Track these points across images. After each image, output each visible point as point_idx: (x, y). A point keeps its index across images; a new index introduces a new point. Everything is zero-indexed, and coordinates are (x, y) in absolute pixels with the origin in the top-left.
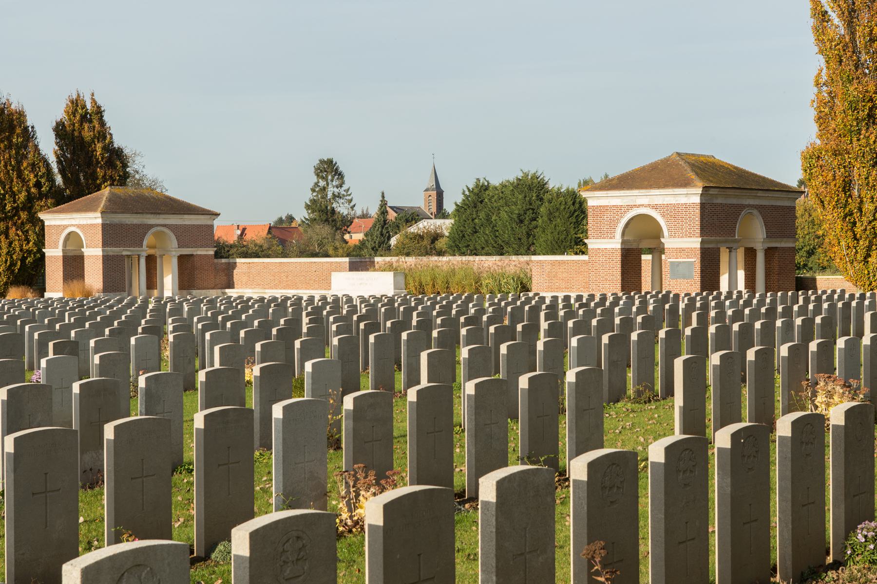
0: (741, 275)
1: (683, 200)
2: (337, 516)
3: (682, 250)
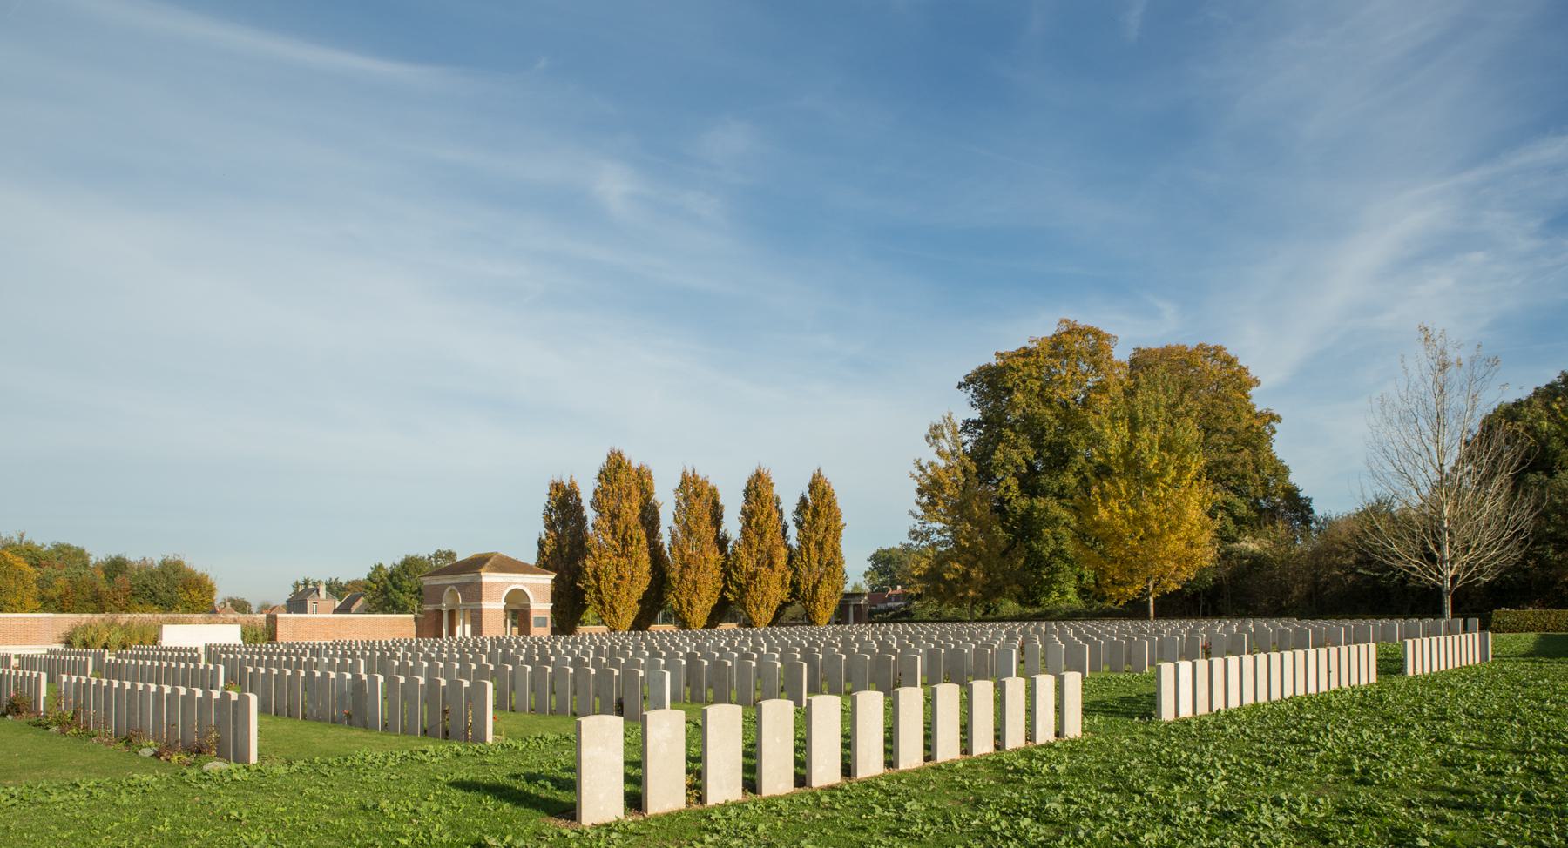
0: (468, 627)
1: (541, 582)
2: (1290, 592)
3: (540, 610)
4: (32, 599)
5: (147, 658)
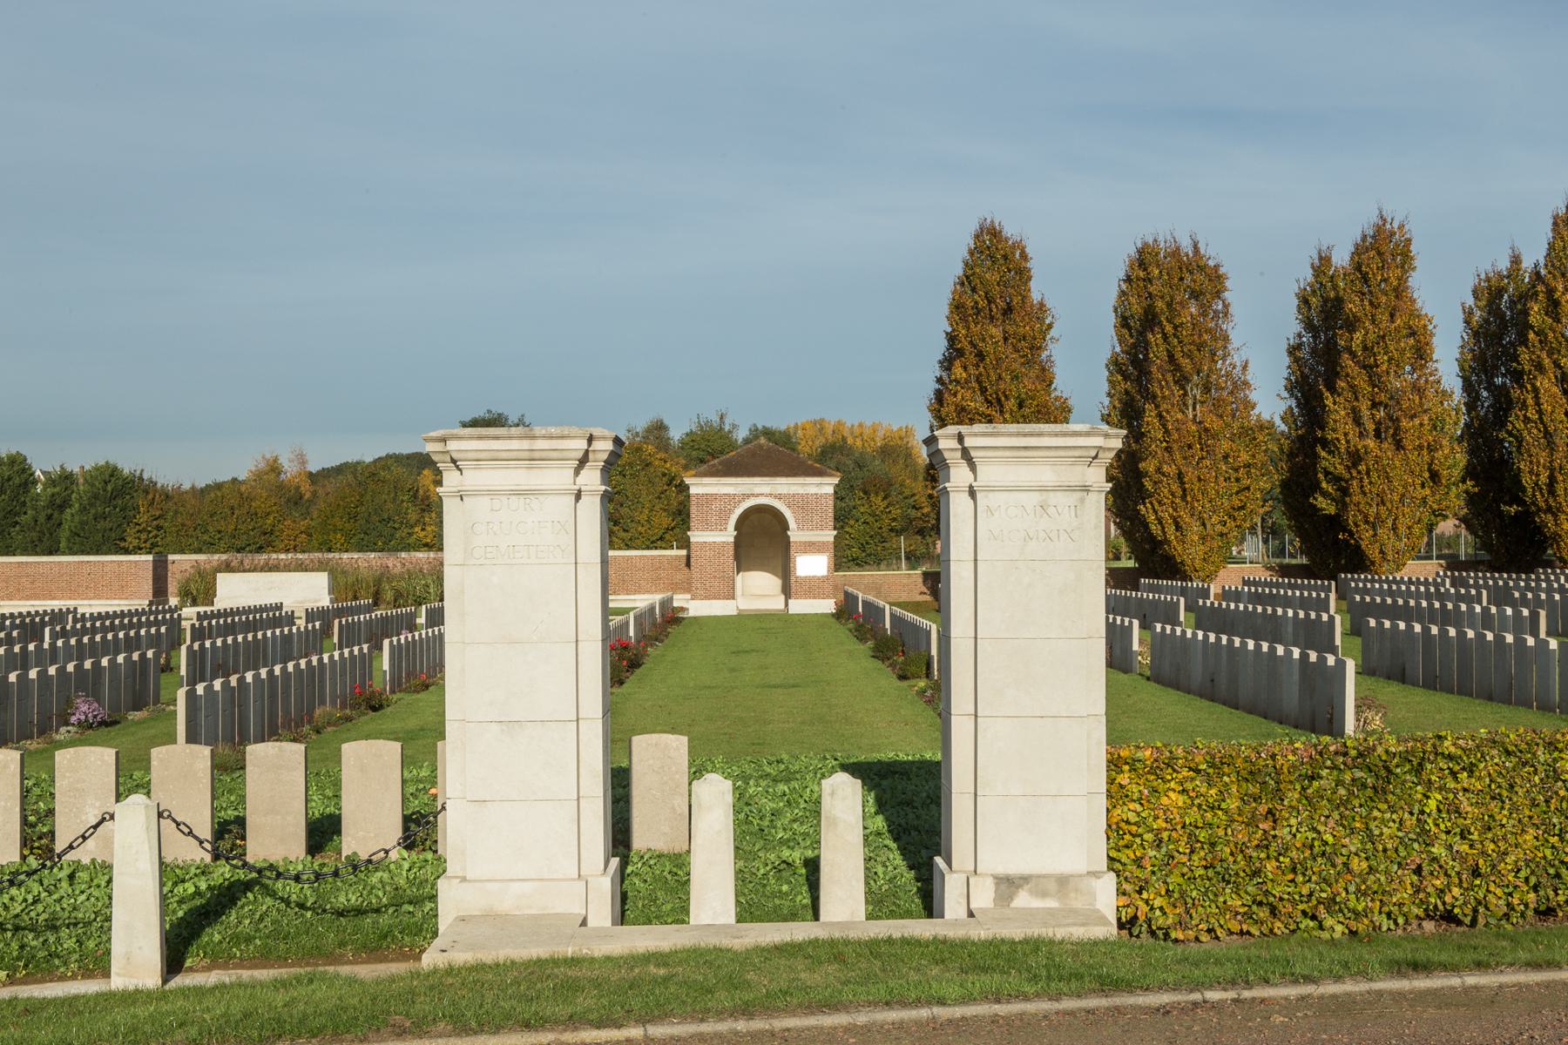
1: (813, 490)
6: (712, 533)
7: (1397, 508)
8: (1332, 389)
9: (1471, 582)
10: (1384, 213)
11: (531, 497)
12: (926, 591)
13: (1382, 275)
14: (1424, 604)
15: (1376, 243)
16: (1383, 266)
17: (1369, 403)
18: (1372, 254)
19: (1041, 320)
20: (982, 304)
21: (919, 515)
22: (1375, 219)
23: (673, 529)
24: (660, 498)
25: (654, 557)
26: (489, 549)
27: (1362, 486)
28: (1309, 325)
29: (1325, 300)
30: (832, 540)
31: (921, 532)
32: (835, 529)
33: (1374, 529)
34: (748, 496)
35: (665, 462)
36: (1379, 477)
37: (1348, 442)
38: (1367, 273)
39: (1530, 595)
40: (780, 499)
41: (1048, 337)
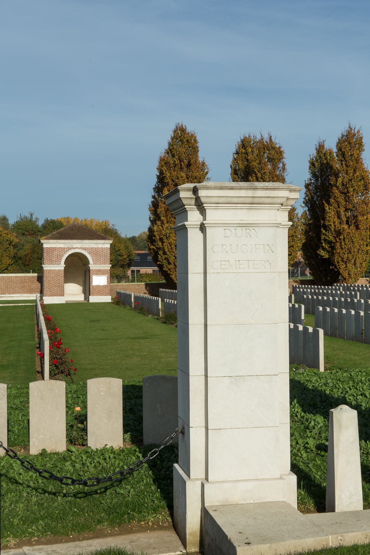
1: (101, 246)
4: (8, 258)
5: (319, 294)
6: (54, 265)
7: (356, 255)
8: (329, 203)
9: (352, 288)
10: (351, 126)
11: (250, 228)
12: (146, 292)
13: (351, 153)
14: (310, 297)
15: (347, 138)
16: (351, 149)
17: (344, 209)
18: (346, 143)
19: (203, 170)
20: (177, 162)
21: (122, 259)
22: (347, 128)
23: (11, 265)
24: (5, 251)
25: (22, 277)
26: (223, 263)
27: (341, 245)
28: (314, 175)
29: (322, 164)
30: (109, 269)
31: (122, 266)
32: (110, 264)
33: (346, 264)
34: (71, 249)
35: (8, 235)
36: (349, 241)
37: (335, 226)
38: (344, 152)
39: (353, 293)
40: (85, 250)
41: (206, 178)
